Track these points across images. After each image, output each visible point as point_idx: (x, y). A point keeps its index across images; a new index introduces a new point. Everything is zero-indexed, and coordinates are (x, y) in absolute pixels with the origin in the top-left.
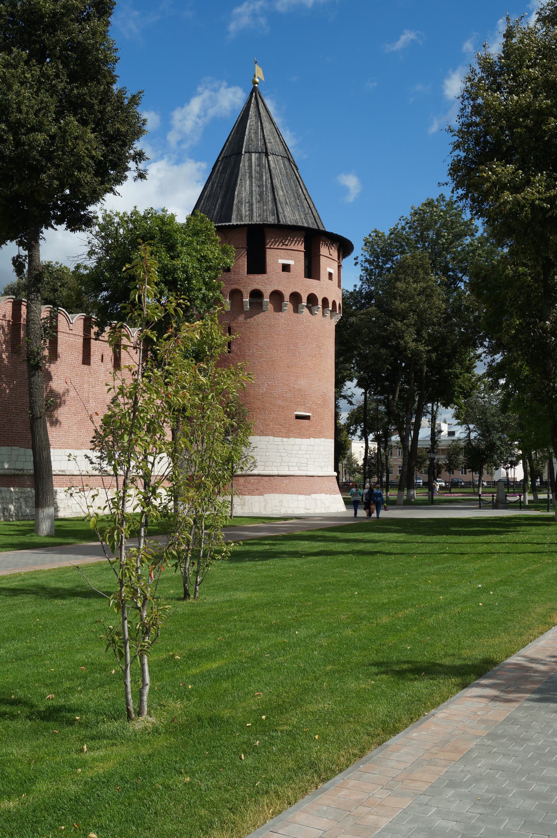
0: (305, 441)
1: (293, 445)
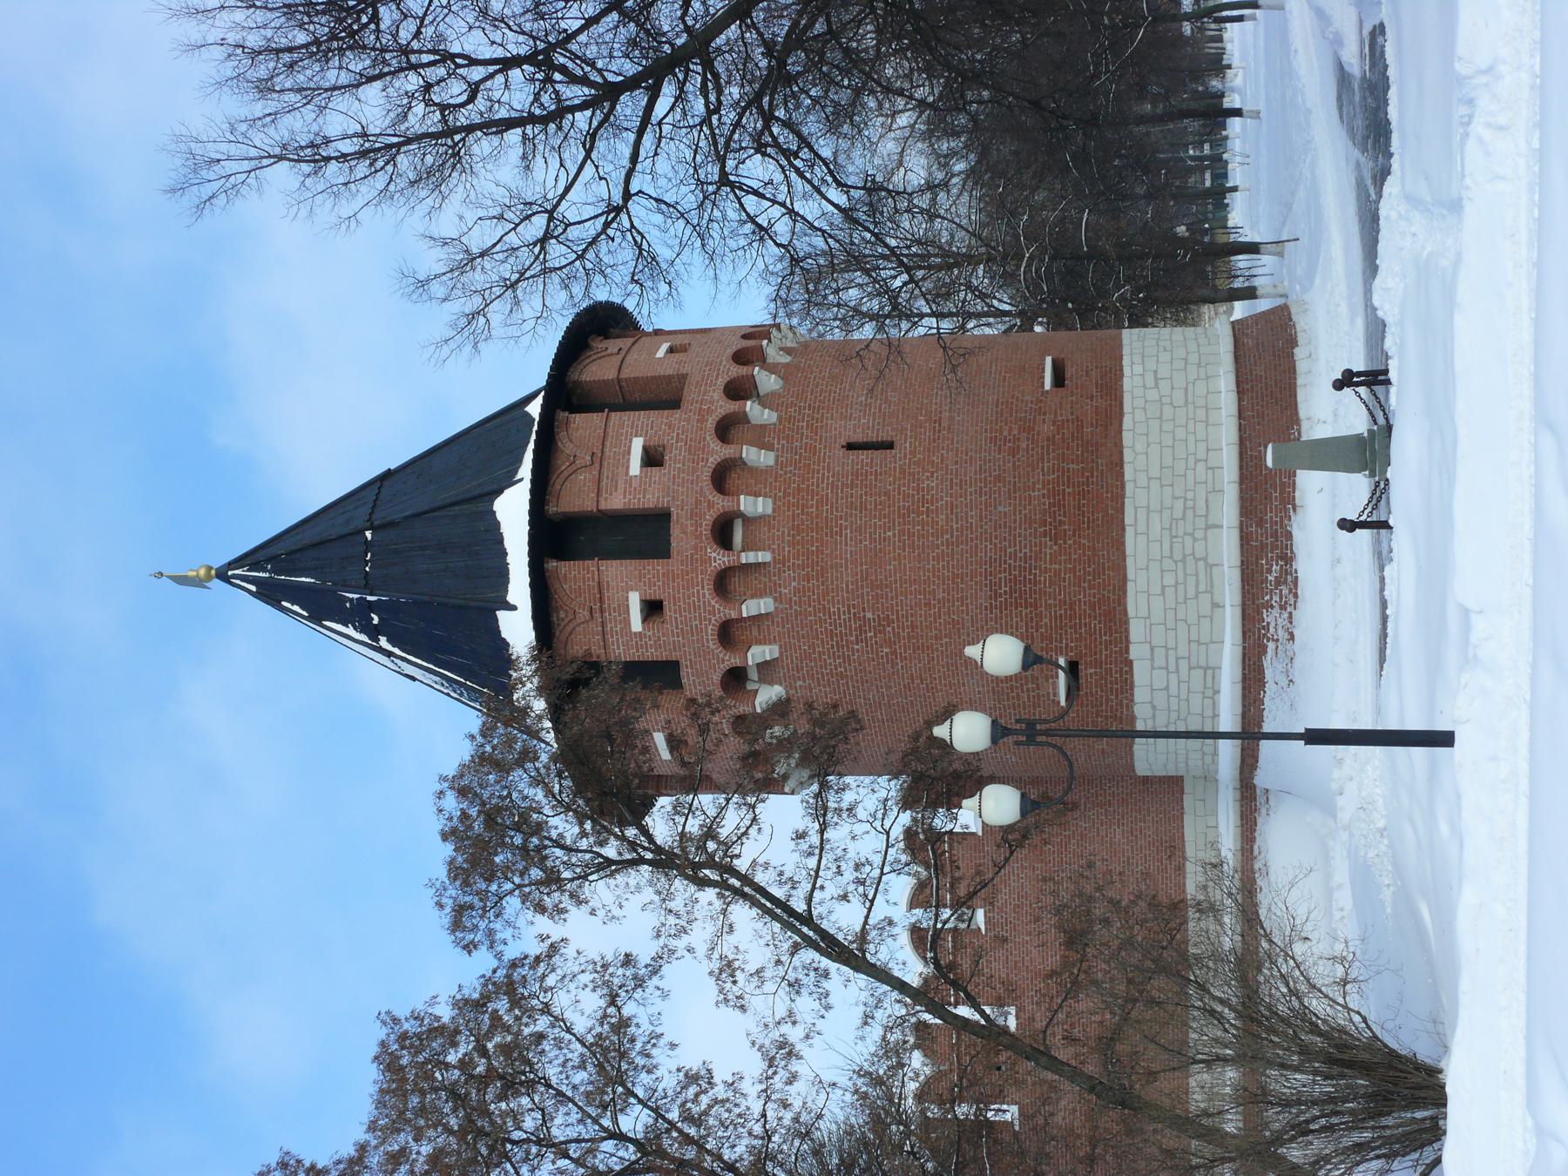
1: (1154, 707)
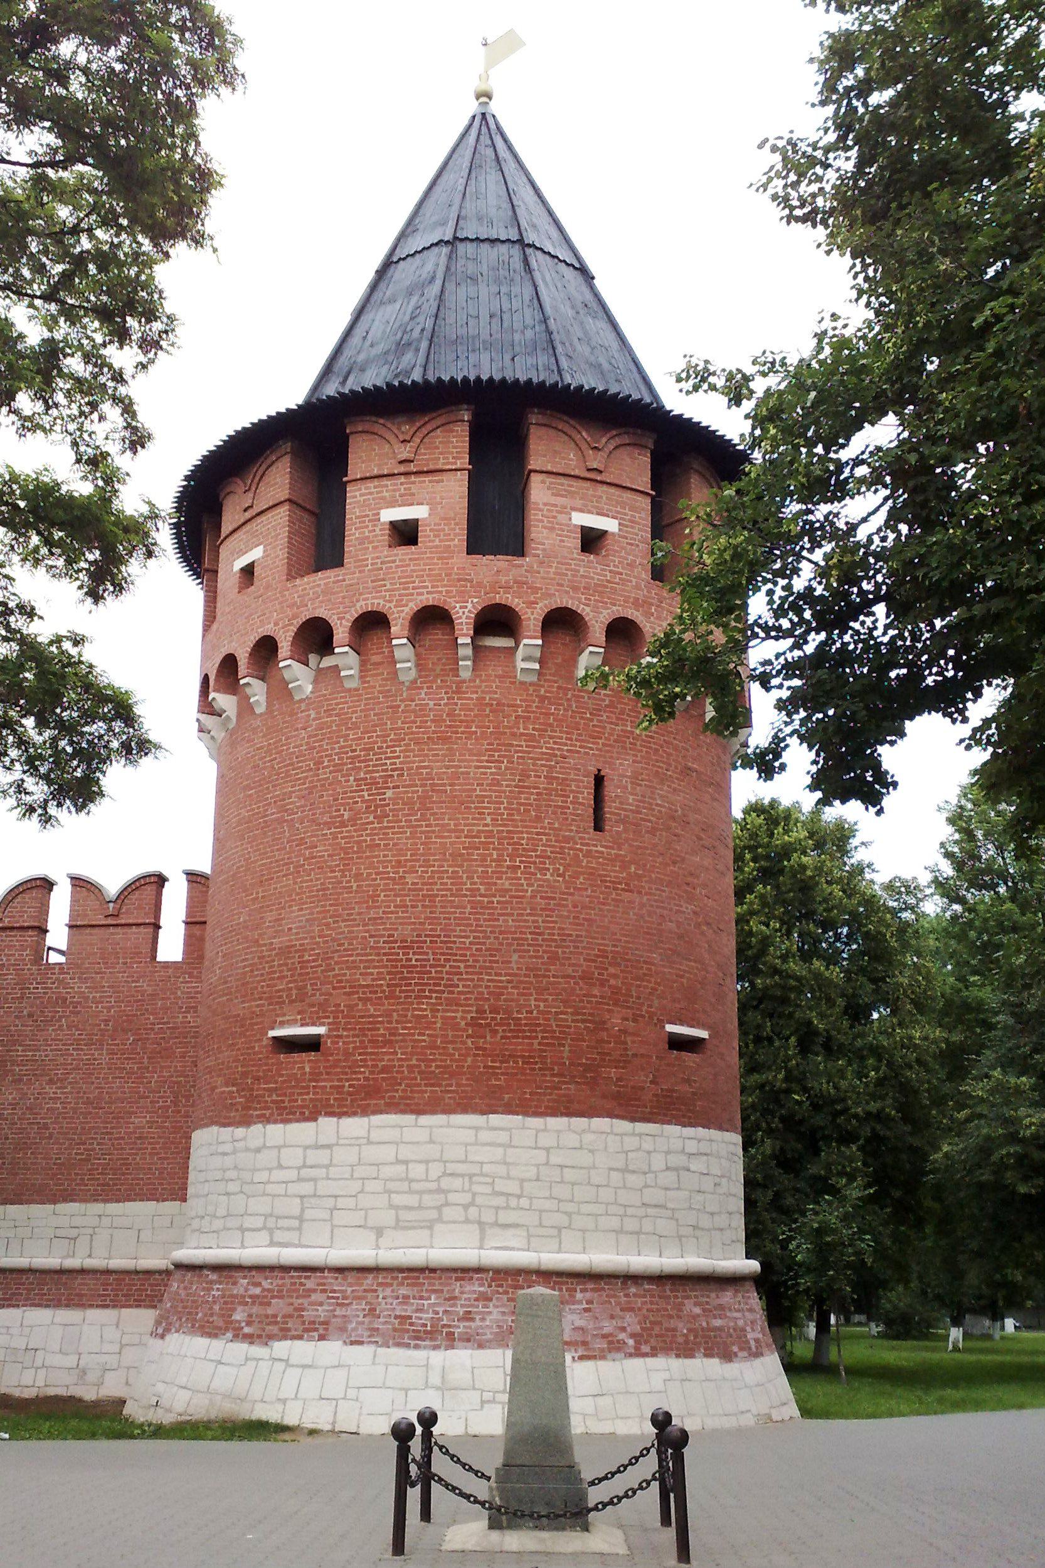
0: (301, 1132)
1: (258, 1150)
